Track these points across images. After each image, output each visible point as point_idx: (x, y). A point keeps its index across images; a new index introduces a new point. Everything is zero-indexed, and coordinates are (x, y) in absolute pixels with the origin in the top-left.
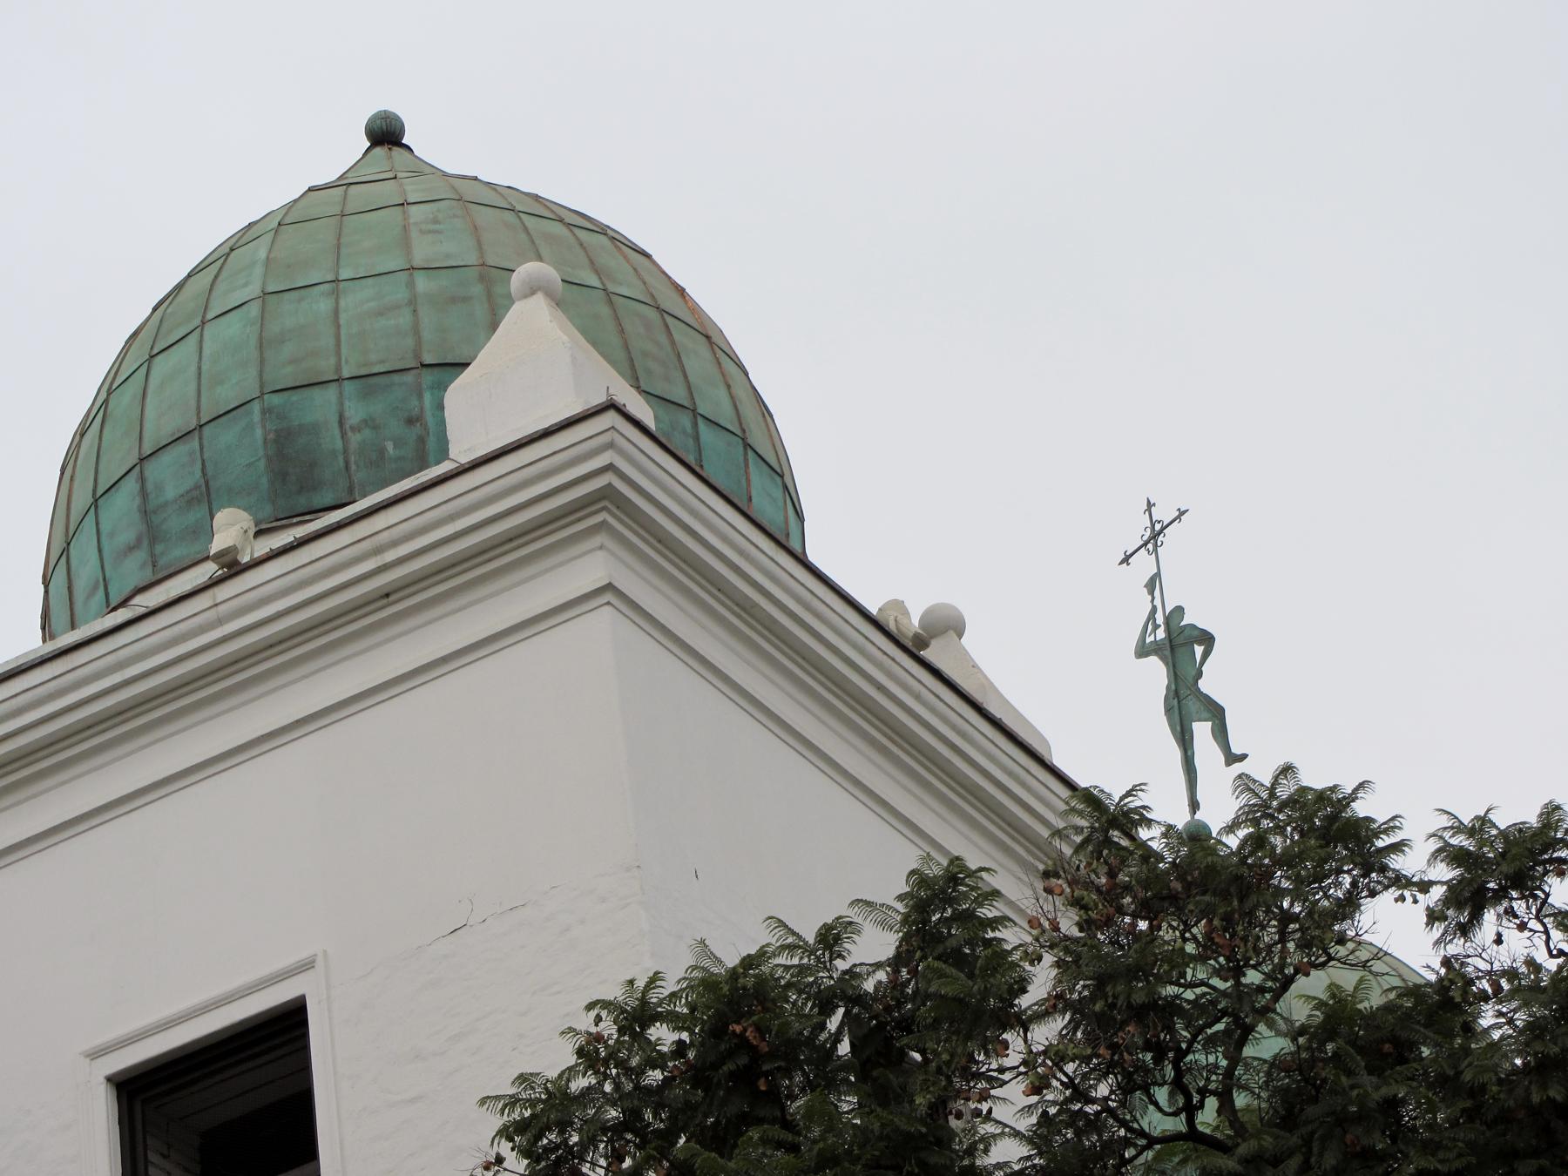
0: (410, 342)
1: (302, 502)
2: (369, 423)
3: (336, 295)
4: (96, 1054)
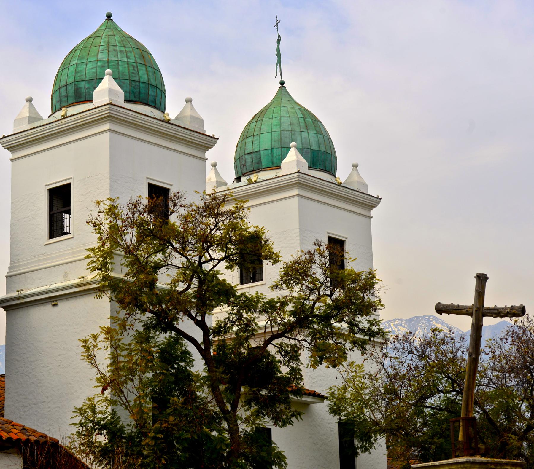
0: (95, 74)
1: (79, 100)
2: (88, 88)
3: (86, 64)
4: (46, 185)
